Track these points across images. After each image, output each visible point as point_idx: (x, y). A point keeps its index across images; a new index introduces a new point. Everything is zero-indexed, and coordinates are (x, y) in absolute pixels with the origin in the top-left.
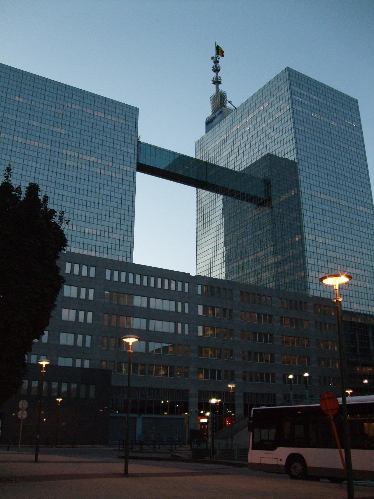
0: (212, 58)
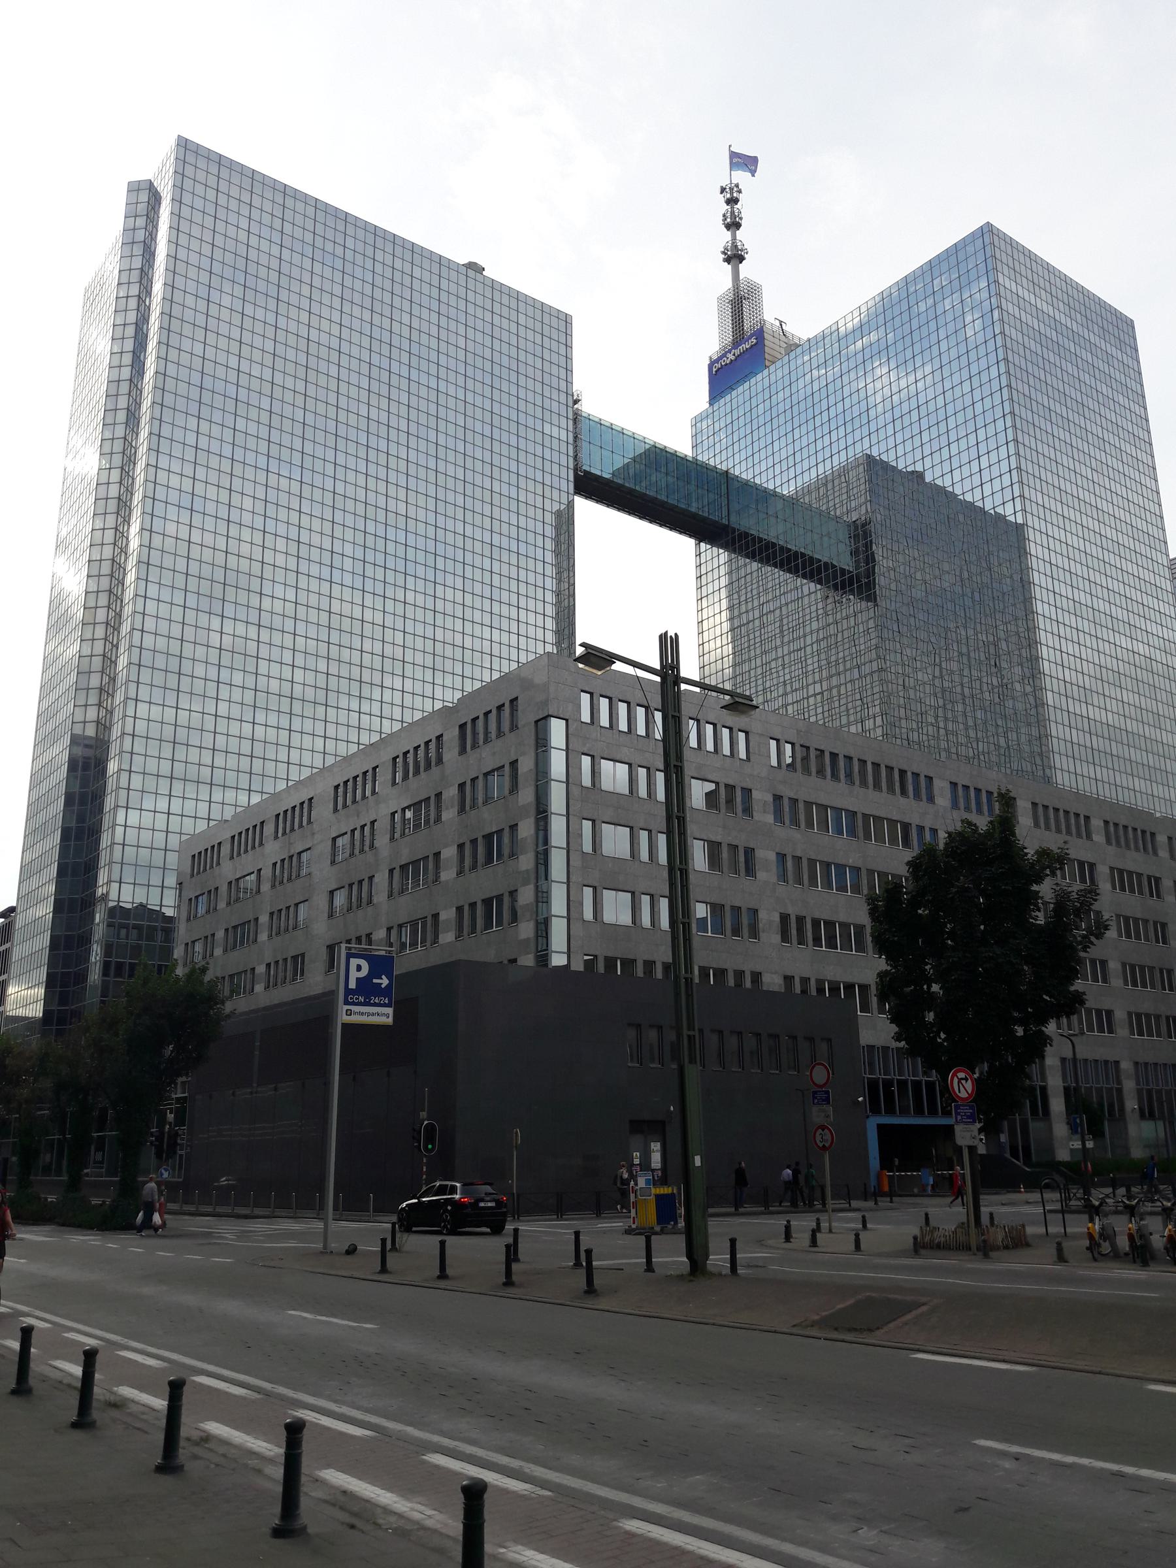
0: (723, 190)
